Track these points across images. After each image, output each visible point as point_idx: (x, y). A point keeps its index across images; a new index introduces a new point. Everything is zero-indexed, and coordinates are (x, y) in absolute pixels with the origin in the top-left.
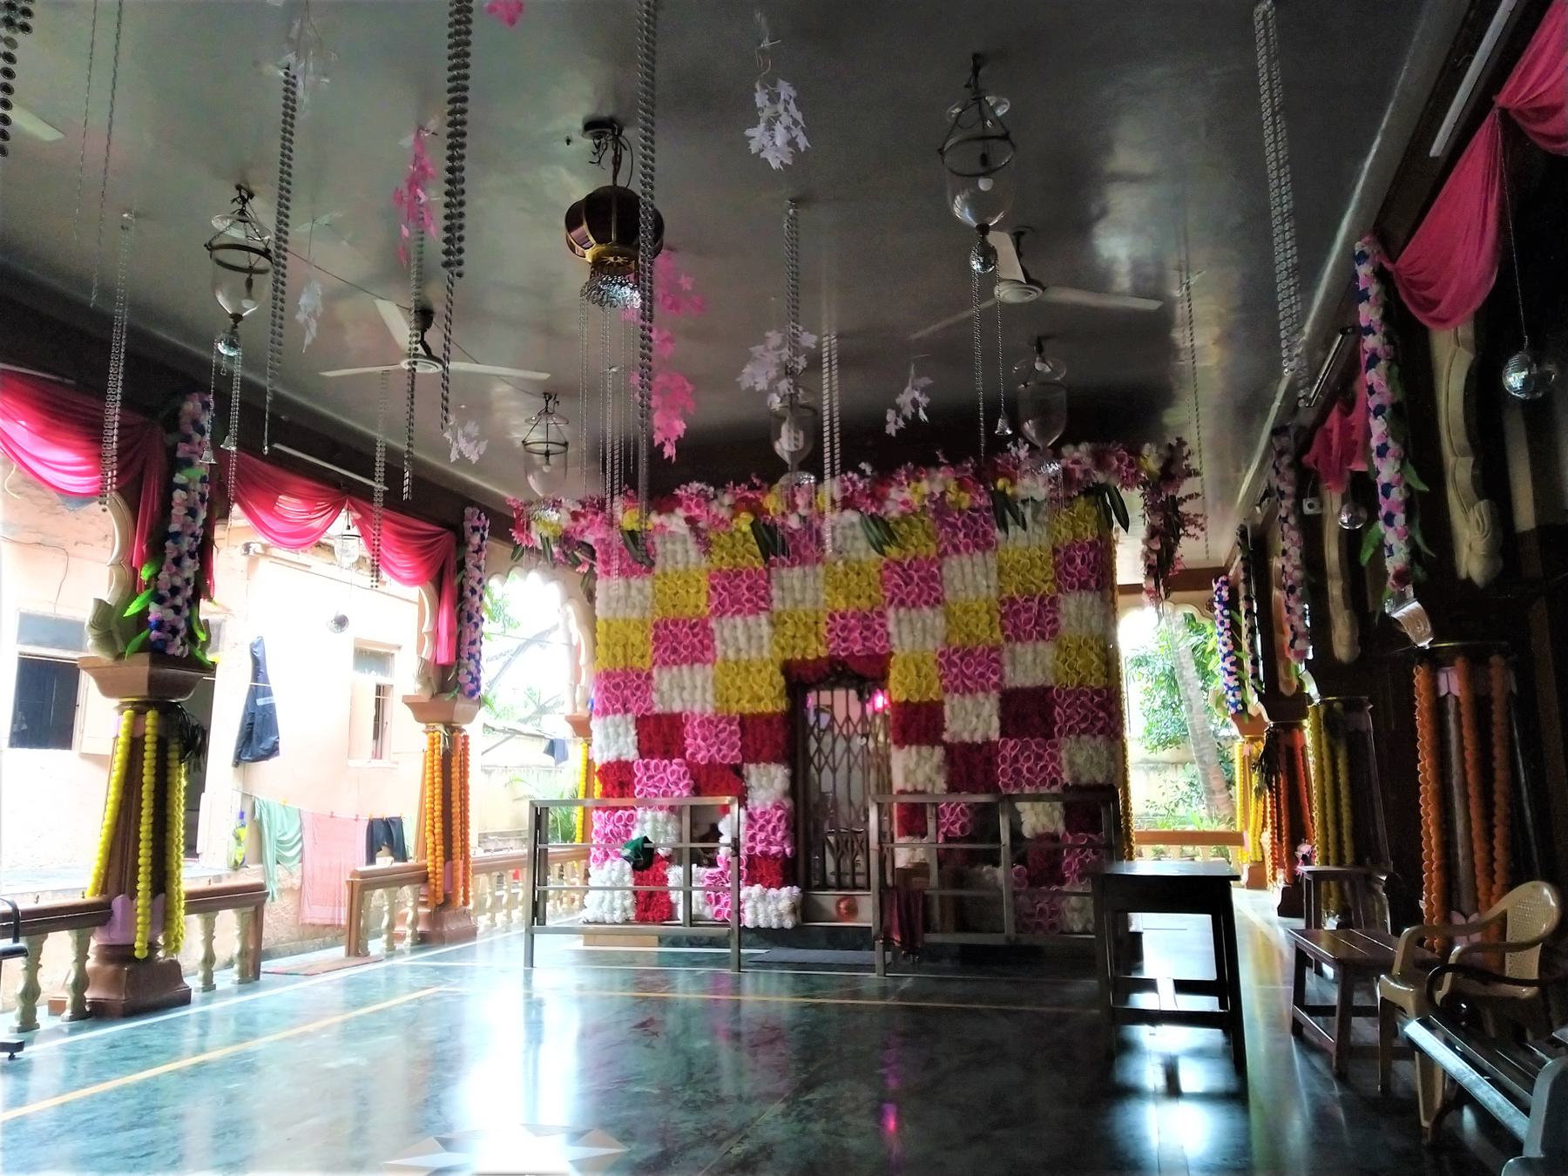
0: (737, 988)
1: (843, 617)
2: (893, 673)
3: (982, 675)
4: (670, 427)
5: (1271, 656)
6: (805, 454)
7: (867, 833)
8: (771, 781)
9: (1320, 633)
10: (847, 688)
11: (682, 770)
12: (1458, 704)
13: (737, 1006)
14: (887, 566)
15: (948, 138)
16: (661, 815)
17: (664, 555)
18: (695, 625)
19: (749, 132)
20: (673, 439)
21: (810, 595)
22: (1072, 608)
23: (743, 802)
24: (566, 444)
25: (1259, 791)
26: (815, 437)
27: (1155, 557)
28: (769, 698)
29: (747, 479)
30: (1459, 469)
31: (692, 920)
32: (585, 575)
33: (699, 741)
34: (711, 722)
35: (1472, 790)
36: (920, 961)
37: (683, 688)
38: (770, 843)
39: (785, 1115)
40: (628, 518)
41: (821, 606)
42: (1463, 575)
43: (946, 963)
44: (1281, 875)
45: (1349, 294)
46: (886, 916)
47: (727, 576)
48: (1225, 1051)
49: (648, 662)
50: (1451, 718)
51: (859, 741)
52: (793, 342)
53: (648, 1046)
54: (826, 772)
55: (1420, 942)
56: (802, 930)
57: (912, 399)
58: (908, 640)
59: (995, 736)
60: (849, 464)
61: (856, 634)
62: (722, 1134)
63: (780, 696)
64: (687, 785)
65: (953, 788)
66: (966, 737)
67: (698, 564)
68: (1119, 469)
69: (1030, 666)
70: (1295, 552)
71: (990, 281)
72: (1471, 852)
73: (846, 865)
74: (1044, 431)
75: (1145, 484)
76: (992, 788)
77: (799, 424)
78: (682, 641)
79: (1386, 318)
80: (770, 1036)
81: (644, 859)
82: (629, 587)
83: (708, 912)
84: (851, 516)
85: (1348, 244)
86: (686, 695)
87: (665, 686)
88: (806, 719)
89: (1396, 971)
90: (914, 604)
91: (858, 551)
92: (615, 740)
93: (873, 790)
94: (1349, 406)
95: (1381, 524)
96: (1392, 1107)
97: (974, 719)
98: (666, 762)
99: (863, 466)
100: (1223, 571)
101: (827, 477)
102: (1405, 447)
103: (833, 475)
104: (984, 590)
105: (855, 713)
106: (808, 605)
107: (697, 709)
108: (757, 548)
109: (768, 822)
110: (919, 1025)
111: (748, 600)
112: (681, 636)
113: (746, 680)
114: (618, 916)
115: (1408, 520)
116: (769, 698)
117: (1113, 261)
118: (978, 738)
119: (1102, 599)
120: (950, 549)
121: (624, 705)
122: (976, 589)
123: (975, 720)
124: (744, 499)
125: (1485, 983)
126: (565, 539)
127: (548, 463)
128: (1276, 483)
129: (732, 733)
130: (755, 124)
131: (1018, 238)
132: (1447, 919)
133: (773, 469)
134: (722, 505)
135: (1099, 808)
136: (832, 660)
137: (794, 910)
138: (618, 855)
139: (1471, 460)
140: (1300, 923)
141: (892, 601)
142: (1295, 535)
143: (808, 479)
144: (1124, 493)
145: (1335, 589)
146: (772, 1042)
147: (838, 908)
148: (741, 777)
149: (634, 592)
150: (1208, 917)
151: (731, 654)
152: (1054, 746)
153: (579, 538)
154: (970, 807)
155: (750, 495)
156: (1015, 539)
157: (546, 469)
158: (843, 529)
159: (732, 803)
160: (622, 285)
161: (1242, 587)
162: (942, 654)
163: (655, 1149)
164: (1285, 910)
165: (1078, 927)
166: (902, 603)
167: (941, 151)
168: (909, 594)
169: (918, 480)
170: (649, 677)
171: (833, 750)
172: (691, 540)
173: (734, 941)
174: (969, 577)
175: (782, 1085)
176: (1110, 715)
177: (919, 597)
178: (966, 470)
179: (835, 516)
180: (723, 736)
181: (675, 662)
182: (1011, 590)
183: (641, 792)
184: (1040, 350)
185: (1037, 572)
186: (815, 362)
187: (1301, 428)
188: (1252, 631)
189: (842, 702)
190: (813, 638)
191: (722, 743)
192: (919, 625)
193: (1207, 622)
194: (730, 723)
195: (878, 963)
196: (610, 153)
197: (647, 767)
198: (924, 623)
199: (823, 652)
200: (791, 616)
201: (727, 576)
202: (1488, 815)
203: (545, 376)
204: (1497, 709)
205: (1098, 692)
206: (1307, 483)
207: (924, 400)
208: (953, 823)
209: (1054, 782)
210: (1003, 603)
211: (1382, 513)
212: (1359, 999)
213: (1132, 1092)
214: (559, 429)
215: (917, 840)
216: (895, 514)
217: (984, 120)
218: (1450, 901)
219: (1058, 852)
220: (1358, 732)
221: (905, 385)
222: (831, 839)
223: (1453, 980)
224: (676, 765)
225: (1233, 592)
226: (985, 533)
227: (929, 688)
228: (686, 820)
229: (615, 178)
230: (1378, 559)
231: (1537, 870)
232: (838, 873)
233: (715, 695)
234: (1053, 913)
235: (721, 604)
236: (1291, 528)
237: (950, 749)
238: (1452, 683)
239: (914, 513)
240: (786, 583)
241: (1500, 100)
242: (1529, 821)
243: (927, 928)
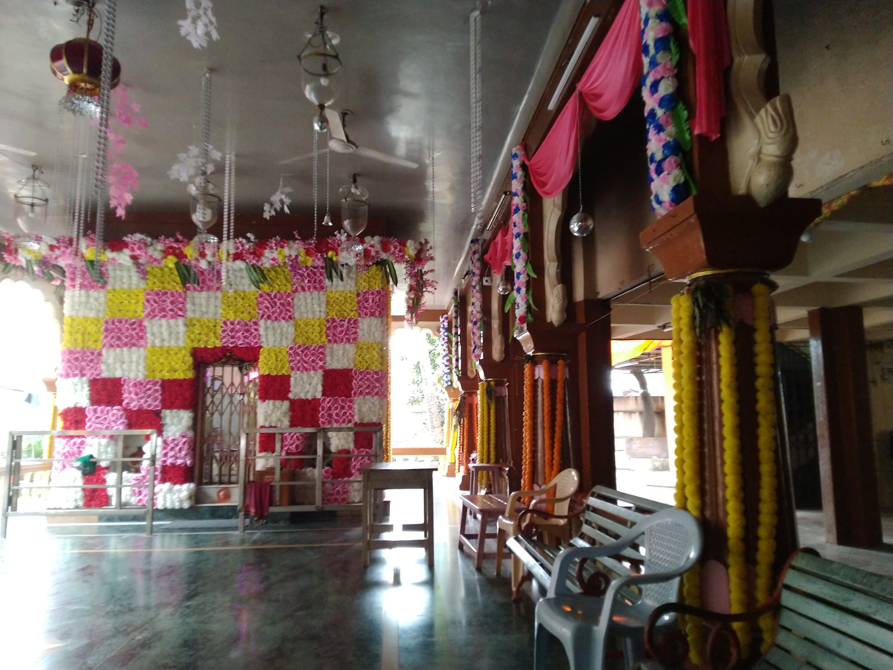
0: (150, 544)
1: (232, 323)
2: (261, 358)
3: (313, 361)
4: (121, 198)
5: (465, 358)
6: (211, 225)
7: (239, 450)
8: (180, 421)
9: (487, 347)
10: (233, 365)
11: (121, 413)
12: (543, 383)
13: (149, 555)
14: (261, 296)
15: (304, 50)
16: (104, 441)
17: (114, 278)
18: (134, 323)
19: (181, 22)
20: (124, 205)
21: (212, 309)
22: (365, 327)
23: (160, 433)
24: (46, 200)
25: (455, 427)
26: (219, 214)
27: (411, 302)
28: (182, 371)
29: (173, 236)
30: (551, 268)
31: (121, 505)
32: (58, 287)
33: (133, 396)
34: (141, 384)
35: (546, 425)
36: (266, 523)
37: (123, 362)
38: (177, 458)
39: (172, 615)
40: (88, 250)
41: (218, 316)
42: (549, 320)
43: (282, 524)
44: (462, 469)
45: (509, 176)
46: (247, 499)
47: (157, 294)
48: (425, 560)
49: (100, 345)
50: (539, 389)
51: (238, 398)
52: (206, 154)
53: (85, 582)
54: (216, 416)
55: (519, 499)
56: (196, 508)
57: (280, 199)
58: (271, 339)
59: (319, 395)
60: (239, 233)
61: (240, 334)
62: (129, 630)
63: (188, 369)
64: (123, 423)
65: (293, 424)
66: (302, 396)
67: (138, 285)
68: (394, 253)
69: (340, 357)
70: (478, 304)
71: (324, 138)
72: (544, 455)
73: (225, 470)
74: (355, 227)
75: (407, 262)
76: (315, 424)
77: (208, 204)
78: (124, 332)
79: (524, 189)
80: (169, 570)
81: (91, 469)
82: (88, 296)
83: (134, 500)
84: (240, 264)
85: (510, 149)
86: (125, 366)
87: (111, 361)
88: (205, 384)
89: (507, 514)
90: (276, 319)
91: (244, 285)
92: (77, 394)
93: (245, 426)
94: (505, 233)
95: (515, 292)
96: (499, 583)
97: (307, 385)
98: (109, 408)
99: (249, 235)
100: (446, 312)
101: (225, 239)
102: (528, 254)
103: (229, 238)
104: (318, 313)
105: (237, 381)
106: (211, 315)
107: (132, 375)
108: (178, 279)
109: (177, 445)
110: (261, 558)
111: (172, 310)
112: (124, 330)
113: (167, 359)
114: (72, 505)
115: (527, 291)
116: (182, 371)
117: (397, 139)
118: (309, 397)
119: (382, 322)
120: (299, 288)
121: (81, 371)
122: (313, 312)
123: (308, 387)
124: (171, 247)
125: (546, 519)
126: (44, 263)
127: (33, 211)
128: (472, 268)
129: (156, 391)
130: (185, 17)
131: (344, 115)
132: (531, 488)
133: (190, 231)
134: (155, 250)
135: (371, 436)
136: (224, 349)
137: (190, 498)
138: (72, 466)
139: (556, 264)
140: (468, 493)
141: (263, 316)
142: (478, 295)
143: (214, 240)
144: (396, 266)
145: (495, 324)
146: (169, 574)
147: (218, 495)
148: (160, 418)
149: (92, 300)
150: (422, 490)
151: (158, 343)
152: (351, 401)
153: (54, 263)
154: (302, 435)
155: (175, 245)
156: (337, 286)
157: (31, 215)
158: (235, 273)
159: (152, 433)
160: (89, 102)
161: (454, 321)
162: (291, 348)
163: (84, 642)
164: (464, 486)
165: (357, 500)
166: (269, 317)
167: (299, 57)
168: (273, 313)
169: (282, 247)
170: (100, 354)
171: (221, 402)
172: (134, 270)
173: (149, 517)
174: (310, 305)
175: (173, 598)
176: (382, 385)
177: (280, 315)
178: (311, 244)
179: (230, 263)
180: (149, 392)
181: (118, 346)
182: (333, 314)
183: (90, 427)
184: (355, 181)
185: (348, 305)
186: (220, 169)
187: (485, 241)
188: (457, 343)
189: (229, 374)
190: (212, 335)
191: (149, 396)
192: (279, 331)
193: (436, 338)
194: (155, 384)
195: (241, 526)
196: (85, 18)
197: (95, 411)
198: (282, 330)
199: (218, 344)
200: (199, 321)
201: (157, 294)
202: (552, 438)
203: (33, 154)
204: (560, 385)
205: (376, 373)
206: (486, 270)
207: (287, 201)
208: (291, 444)
209: (350, 421)
210: (328, 321)
211: (516, 287)
212: (489, 530)
213: (378, 584)
214: (41, 190)
215: (270, 454)
216: (267, 265)
217: (325, 44)
218: (533, 480)
219: (349, 459)
220: (501, 396)
221: (277, 190)
222: (217, 455)
223: (531, 518)
224: (116, 410)
225: (450, 323)
226: (320, 281)
227: (282, 368)
228: (121, 444)
229: (89, 30)
230: (513, 309)
231: (572, 463)
232: (220, 475)
233: (145, 367)
234: (345, 493)
235: (153, 311)
236: (477, 292)
237: (293, 402)
238: (541, 372)
239: (279, 266)
240: (197, 301)
241: (579, 86)
242: (570, 440)
243: (271, 504)
